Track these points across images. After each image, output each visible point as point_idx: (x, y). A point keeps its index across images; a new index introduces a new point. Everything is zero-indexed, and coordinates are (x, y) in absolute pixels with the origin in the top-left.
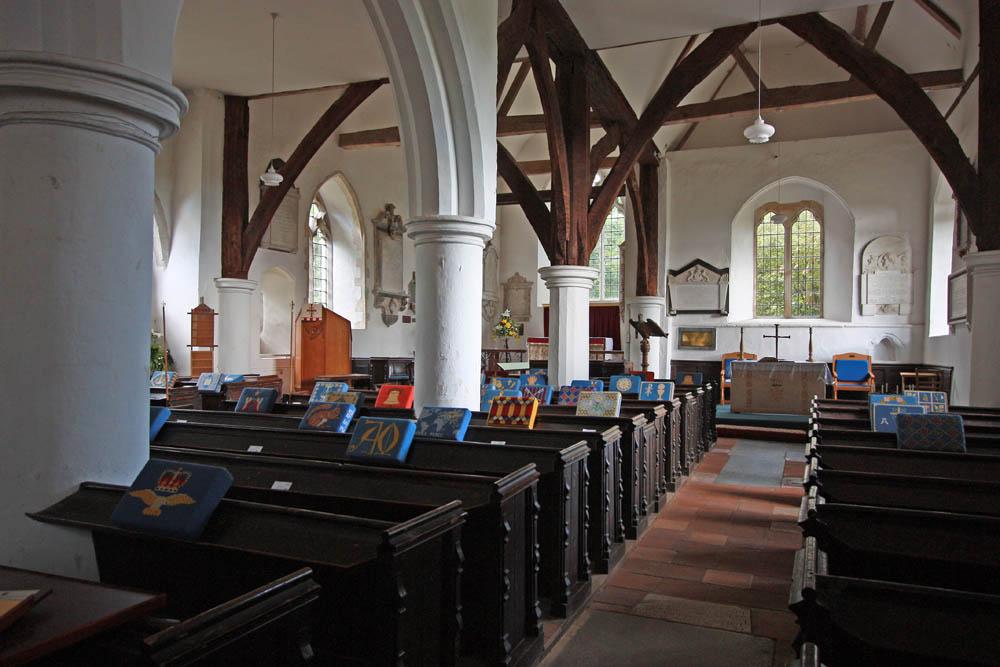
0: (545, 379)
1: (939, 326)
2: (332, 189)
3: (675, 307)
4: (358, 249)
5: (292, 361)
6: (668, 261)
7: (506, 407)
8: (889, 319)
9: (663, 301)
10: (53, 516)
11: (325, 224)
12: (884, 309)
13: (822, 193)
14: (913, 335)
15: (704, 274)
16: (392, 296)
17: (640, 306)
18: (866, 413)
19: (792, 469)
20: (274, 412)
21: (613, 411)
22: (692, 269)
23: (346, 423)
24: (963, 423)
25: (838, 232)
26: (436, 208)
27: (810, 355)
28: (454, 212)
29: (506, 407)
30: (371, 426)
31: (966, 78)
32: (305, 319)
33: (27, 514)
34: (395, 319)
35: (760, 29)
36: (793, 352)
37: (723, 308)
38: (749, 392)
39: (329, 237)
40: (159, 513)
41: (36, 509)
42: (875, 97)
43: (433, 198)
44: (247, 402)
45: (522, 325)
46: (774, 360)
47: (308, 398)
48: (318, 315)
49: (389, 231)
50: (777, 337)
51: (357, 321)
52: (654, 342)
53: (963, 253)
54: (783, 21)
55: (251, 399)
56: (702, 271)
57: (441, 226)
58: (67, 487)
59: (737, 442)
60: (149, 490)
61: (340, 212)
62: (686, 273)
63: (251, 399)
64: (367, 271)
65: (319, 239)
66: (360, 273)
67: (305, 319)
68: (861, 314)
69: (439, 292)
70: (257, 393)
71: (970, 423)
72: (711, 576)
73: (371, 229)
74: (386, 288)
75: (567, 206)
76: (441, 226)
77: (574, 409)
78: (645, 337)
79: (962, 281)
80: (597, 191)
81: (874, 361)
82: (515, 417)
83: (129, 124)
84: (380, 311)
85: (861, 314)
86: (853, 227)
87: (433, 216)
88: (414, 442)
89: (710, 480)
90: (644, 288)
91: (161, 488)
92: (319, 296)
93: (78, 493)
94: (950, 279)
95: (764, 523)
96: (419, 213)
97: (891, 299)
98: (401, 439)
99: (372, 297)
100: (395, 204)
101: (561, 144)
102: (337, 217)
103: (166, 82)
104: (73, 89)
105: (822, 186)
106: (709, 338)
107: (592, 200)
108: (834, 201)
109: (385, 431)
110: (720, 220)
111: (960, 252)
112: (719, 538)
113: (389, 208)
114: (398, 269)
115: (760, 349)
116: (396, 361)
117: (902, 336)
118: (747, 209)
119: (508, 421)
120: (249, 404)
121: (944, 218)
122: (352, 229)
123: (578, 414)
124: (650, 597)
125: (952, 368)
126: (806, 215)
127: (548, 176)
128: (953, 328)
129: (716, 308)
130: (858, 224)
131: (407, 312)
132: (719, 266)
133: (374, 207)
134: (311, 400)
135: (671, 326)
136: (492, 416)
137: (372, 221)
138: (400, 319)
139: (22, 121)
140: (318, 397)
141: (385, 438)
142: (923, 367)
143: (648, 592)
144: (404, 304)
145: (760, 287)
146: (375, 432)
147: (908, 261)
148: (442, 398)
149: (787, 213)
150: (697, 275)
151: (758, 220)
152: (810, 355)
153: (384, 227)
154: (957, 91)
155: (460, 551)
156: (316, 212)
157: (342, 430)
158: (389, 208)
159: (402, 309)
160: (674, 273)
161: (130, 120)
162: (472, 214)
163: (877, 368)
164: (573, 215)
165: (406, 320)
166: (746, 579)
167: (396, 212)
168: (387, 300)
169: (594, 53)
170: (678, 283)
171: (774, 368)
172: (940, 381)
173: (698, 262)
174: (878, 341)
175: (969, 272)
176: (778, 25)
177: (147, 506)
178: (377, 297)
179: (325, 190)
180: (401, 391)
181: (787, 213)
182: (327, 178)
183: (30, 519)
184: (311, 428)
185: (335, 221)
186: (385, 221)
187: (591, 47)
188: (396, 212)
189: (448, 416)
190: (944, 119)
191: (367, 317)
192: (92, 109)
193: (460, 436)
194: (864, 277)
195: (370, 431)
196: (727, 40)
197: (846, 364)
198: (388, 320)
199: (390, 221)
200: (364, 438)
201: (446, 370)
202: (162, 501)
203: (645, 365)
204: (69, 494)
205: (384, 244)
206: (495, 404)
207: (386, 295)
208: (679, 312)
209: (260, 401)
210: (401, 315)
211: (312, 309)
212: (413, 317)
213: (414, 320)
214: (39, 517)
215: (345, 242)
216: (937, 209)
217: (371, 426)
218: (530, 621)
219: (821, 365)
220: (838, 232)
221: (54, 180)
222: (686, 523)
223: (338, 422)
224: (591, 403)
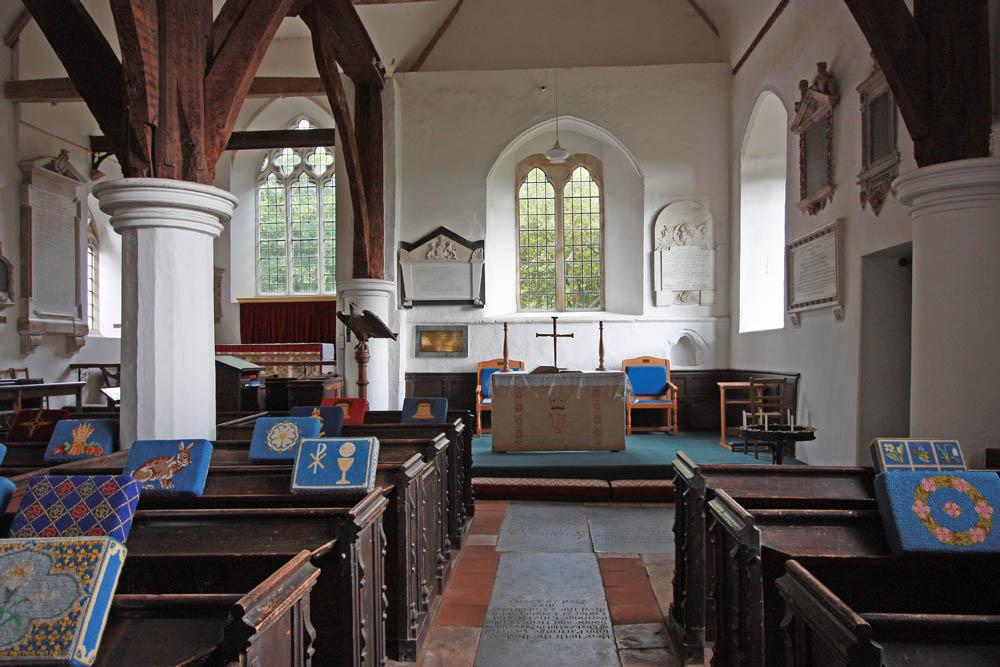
3: (410, 296)
6: (399, 228)
9: (394, 287)
12: (682, 297)
13: (602, 145)
14: (717, 332)
15: (450, 248)
22: (433, 242)
27: (601, 360)
36: (578, 357)
37: (476, 296)
38: (519, 421)
46: (553, 370)
50: (555, 335)
56: (447, 245)
62: (423, 247)
68: (654, 303)
78: (362, 339)
81: (673, 367)
85: (654, 303)
106: (456, 339)
115: (531, 356)
117: (704, 332)
121: (763, 175)
125: (798, 375)
126: (581, 174)
129: (468, 297)
130: (649, 183)
132: (471, 238)
135: (404, 323)
147: (709, 234)
150: (440, 250)
151: (520, 179)
152: (601, 360)
160: (408, 247)
170: (414, 262)
171: (554, 382)
173: (442, 231)
174: (676, 340)
194: (657, 254)
197: (643, 372)
208: (417, 303)
219: (617, 377)
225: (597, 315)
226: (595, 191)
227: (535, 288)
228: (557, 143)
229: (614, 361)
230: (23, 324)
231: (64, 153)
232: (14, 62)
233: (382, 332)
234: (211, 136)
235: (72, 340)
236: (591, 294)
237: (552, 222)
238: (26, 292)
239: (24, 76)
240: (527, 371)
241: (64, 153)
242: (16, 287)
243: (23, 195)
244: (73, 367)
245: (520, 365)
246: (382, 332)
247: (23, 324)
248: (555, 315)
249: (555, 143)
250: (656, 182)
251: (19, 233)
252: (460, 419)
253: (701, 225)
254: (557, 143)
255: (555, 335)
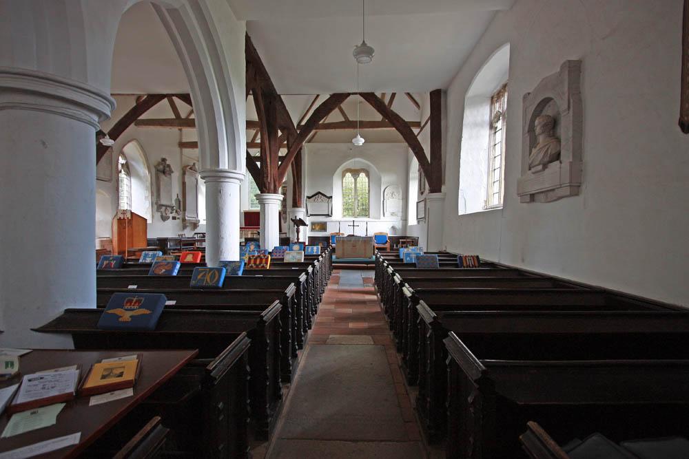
0: (259, 246)
1: (412, 220)
2: (131, 149)
3: (309, 213)
4: (147, 181)
5: (111, 241)
6: (307, 191)
7: (256, 259)
8: (394, 218)
9: (304, 210)
10: (54, 327)
11: (127, 167)
12: (392, 214)
13: (369, 166)
14: (403, 226)
16: (166, 206)
17: (294, 212)
18: (398, 256)
19: (365, 280)
20: (123, 268)
21: (301, 260)
23: (176, 271)
24: (438, 258)
25: (374, 180)
26: (218, 165)
28: (226, 168)
29: (256, 259)
30: (203, 271)
31: (422, 125)
32: (120, 218)
33: (32, 330)
34: (168, 218)
35: (351, 96)
36: (360, 232)
38: (343, 250)
39: (128, 173)
40: (130, 319)
41: (38, 326)
42: (394, 129)
43: (216, 159)
44: (105, 263)
45: (307, 225)
46: (353, 235)
47: (139, 260)
48: (129, 215)
49: (164, 172)
50: (354, 226)
51: (148, 216)
52: (301, 228)
53: (422, 193)
54: (361, 94)
55: (107, 262)
57: (220, 174)
58: (59, 311)
59: (341, 271)
60: (120, 309)
61: (133, 160)
63: (107, 262)
64: (152, 192)
65: (123, 175)
66: (148, 194)
67: (120, 218)
68: (384, 216)
69: (220, 205)
70: (111, 259)
71: (440, 258)
72: (351, 325)
73: (153, 170)
74: (163, 202)
75: (269, 166)
76: (220, 174)
77: (283, 259)
78: (298, 226)
79: (422, 204)
80: (282, 158)
81: (389, 235)
82: (260, 263)
83: (86, 115)
84: (159, 214)
85: (384, 216)
86: (381, 180)
87: (217, 169)
88: (226, 277)
89: (335, 287)
90: (296, 204)
91: (128, 307)
92: (124, 205)
93: (63, 315)
94: (417, 203)
95: (364, 302)
96: (208, 167)
97: (147, 195)
98: (220, 276)
99: (155, 207)
100: (167, 158)
101: (266, 136)
102: (133, 163)
103: (107, 93)
104: (58, 94)
105: (367, 162)
106: (323, 227)
107: (280, 163)
108: (373, 168)
109: (210, 274)
110: (328, 174)
111: (421, 192)
112: (349, 310)
113: (164, 160)
114: (170, 192)
115: (346, 231)
116: (171, 240)
117: (399, 225)
118: (339, 171)
119: (257, 266)
120: (106, 264)
121: (414, 178)
122: (142, 170)
123: (285, 261)
124: (331, 336)
126: (362, 175)
127: (259, 150)
128: (418, 222)
130: (383, 180)
131: (174, 214)
132: (328, 196)
133: (155, 159)
134: (140, 261)
135: (308, 221)
136: (248, 264)
137: (155, 167)
138: (171, 218)
139: (22, 108)
140: (145, 259)
141: (215, 277)
142: (408, 237)
143: (329, 334)
144: (173, 210)
145: (345, 204)
146: (205, 274)
147: (401, 195)
148: (222, 257)
149: (355, 173)
151: (343, 176)
153: (161, 170)
154: (419, 130)
155: (280, 322)
156: (122, 161)
157: (175, 274)
158: (164, 160)
159: (171, 213)
160: (309, 198)
161: (88, 113)
162: (235, 169)
163: (390, 238)
164: (272, 171)
165: (174, 218)
166: (365, 325)
167: (168, 163)
168: (164, 208)
169: (279, 96)
171: (353, 239)
172: (414, 242)
173: (319, 193)
174: (390, 227)
175: (425, 200)
176: (358, 96)
177: (121, 317)
178: (158, 206)
179: (127, 149)
180: (193, 254)
181: (355, 173)
182: (129, 142)
183: (34, 333)
184: (156, 274)
185: (132, 165)
186: (161, 167)
187: (278, 93)
188: (168, 163)
189: (233, 265)
190: (416, 137)
191: (153, 217)
192: (66, 105)
193: (240, 274)
195: (201, 274)
196: (337, 99)
197: (380, 237)
198: (164, 218)
199: (164, 167)
200: (199, 277)
201: (224, 243)
202: (131, 313)
203: (298, 239)
204: (58, 316)
205: (161, 179)
206: (250, 259)
207: (163, 205)
208: (311, 215)
209: (113, 262)
210: (171, 216)
211: (124, 212)
212: (178, 217)
213: (178, 218)
214: (43, 330)
215: (138, 177)
216: (411, 175)
217: (203, 271)
218: (294, 350)
219: (371, 237)
220: (374, 180)
221: (44, 143)
222: (334, 306)
223: (172, 271)
224: (291, 256)
225: (366, 219)
226: (367, 180)
227: (348, 209)
228: (364, 42)
229: (371, 233)
230: (184, 220)
231: (194, 164)
232: (181, 135)
233: (304, 224)
234: (279, 183)
235: (195, 225)
236: (365, 212)
237: (353, 185)
238: (184, 210)
239: (184, 140)
240: (345, 236)
241: (194, 164)
242: (182, 208)
243: (183, 178)
244: (195, 234)
245: (343, 234)
246: (304, 224)
247: (184, 220)
248: (354, 219)
249: (362, 42)
250: (385, 179)
251: (669, 305)
252: (244, 333)
253: (398, 192)
254: (364, 42)
255: (354, 226)
